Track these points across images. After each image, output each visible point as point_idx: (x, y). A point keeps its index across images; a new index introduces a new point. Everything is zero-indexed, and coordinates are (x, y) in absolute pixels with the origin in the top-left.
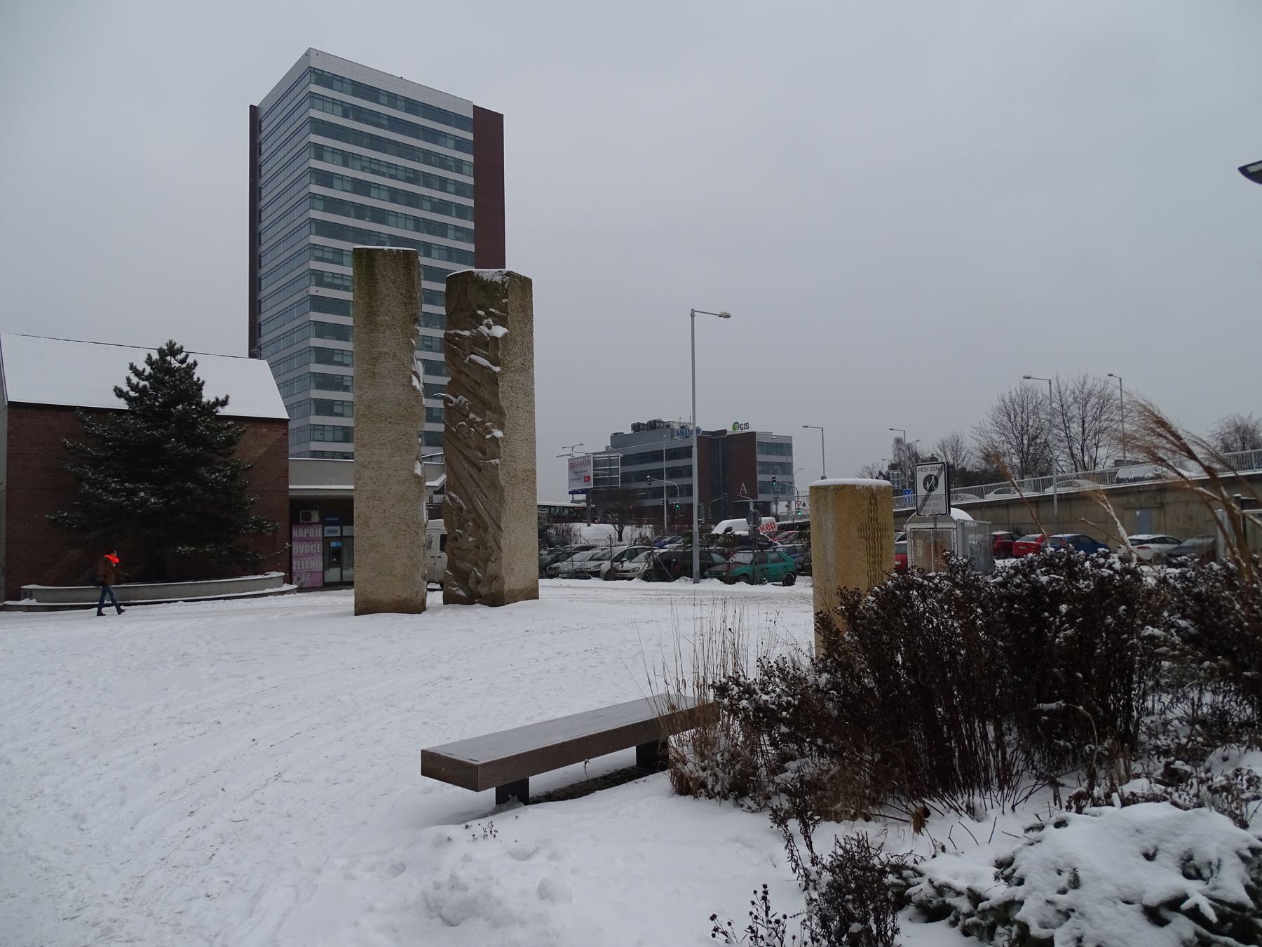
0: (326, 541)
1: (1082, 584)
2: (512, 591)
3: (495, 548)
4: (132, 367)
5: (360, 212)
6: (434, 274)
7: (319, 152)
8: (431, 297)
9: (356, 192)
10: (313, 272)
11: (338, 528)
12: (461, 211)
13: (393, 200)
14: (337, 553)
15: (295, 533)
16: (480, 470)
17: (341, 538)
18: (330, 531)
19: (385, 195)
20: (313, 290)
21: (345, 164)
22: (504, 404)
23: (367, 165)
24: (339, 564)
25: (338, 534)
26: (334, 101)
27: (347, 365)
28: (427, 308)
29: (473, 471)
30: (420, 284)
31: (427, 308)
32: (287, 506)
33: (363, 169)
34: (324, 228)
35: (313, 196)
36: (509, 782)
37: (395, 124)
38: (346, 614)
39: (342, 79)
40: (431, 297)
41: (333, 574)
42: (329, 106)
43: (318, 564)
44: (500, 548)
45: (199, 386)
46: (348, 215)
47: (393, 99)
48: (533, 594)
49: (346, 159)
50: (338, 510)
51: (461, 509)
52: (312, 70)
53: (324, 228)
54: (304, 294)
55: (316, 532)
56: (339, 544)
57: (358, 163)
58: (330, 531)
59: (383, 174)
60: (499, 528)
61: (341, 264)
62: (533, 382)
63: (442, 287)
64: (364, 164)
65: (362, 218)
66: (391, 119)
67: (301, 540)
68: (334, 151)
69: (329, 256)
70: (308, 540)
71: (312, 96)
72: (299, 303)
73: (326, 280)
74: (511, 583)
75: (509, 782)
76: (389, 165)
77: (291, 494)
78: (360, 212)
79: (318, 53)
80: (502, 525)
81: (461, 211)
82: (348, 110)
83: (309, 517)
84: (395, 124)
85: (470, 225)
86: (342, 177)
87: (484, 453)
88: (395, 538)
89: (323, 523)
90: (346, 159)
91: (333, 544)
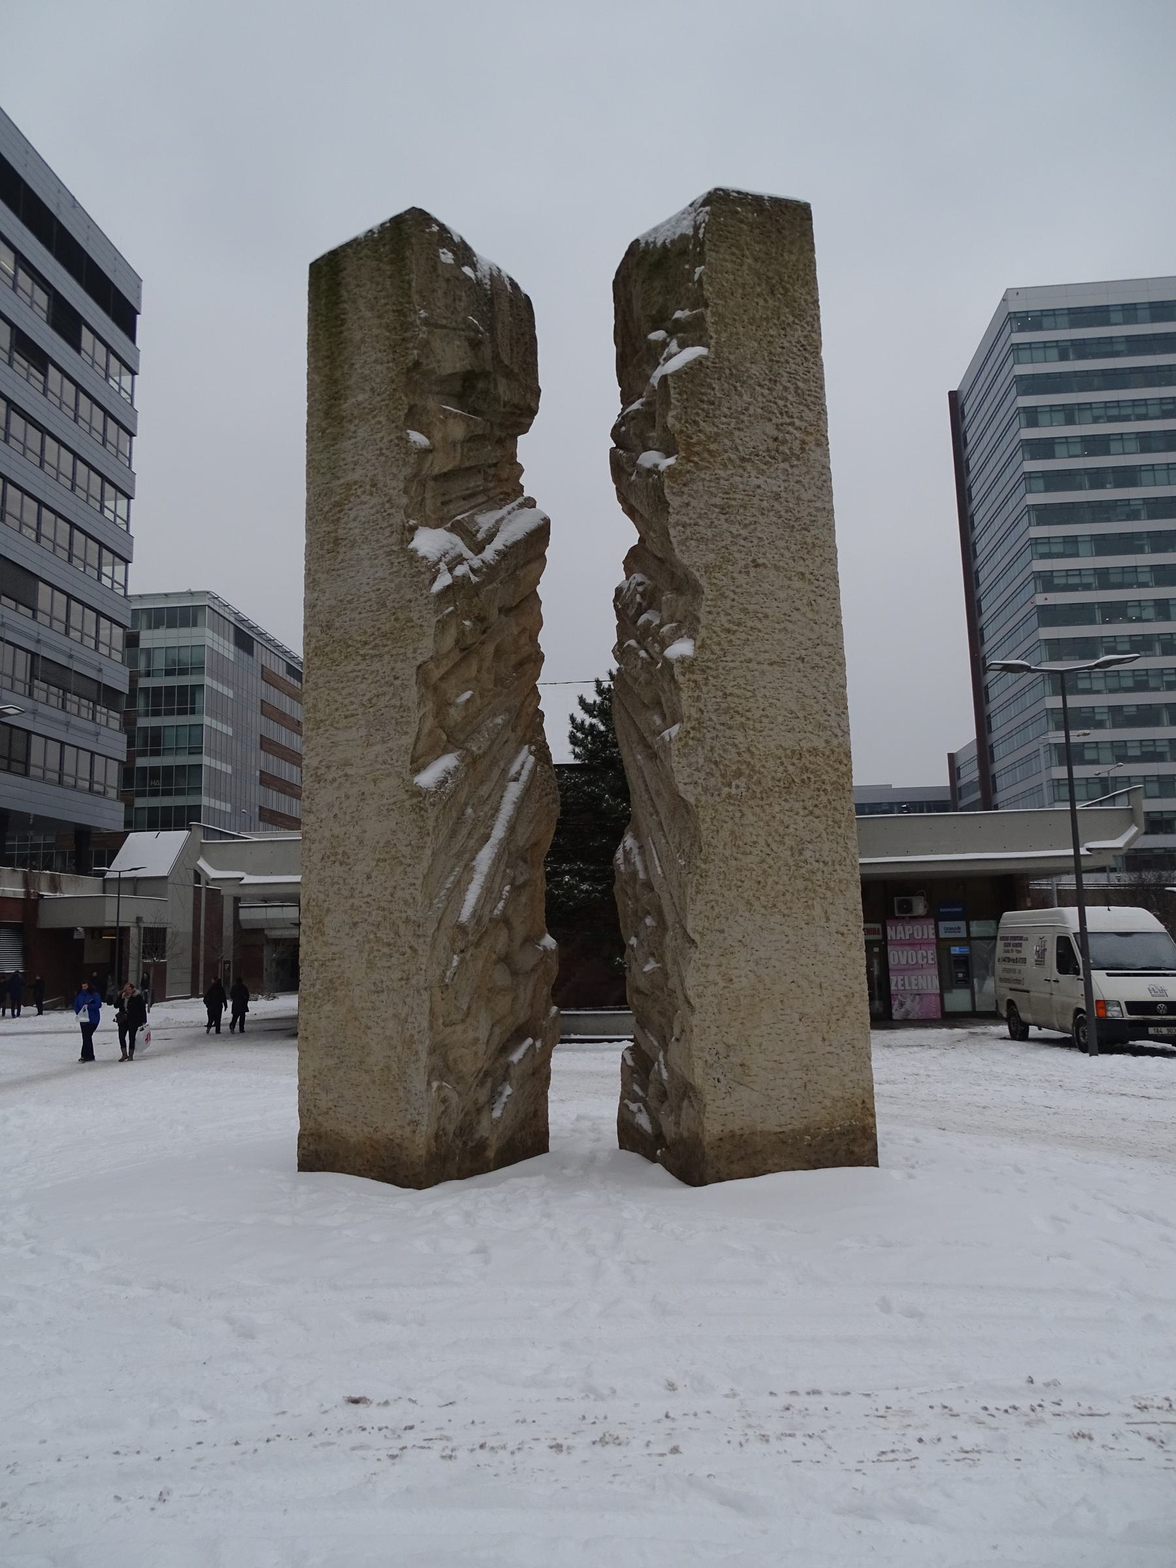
0: (942, 945)
1: (467, 270)
4: (582, 701)
5: (1097, 478)
7: (1032, 416)
9: (1092, 453)
10: (1038, 575)
11: (962, 924)
13: (1145, 449)
14: (963, 962)
15: (891, 933)
17: (968, 940)
18: (948, 930)
19: (1132, 445)
20: (1041, 599)
21: (1070, 421)
23: (1100, 412)
24: (967, 983)
25: (963, 934)
26: (1045, 345)
27: (1098, 692)
33: (1096, 420)
34: (1045, 514)
35: (1029, 476)
37: (1137, 345)
39: (1053, 313)
41: (958, 1000)
42: (1039, 354)
43: (930, 982)
46: (1080, 488)
47: (1130, 312)
49: (1070, 414)
52: (1012, 317)
53: (1045, 514)
54: (1029, 606)
55: (927, 931)
56: (965, 950)
57: (1088, 415)
58: (948, 930)
59: (1126, 418)
61: (1077, 555)
64: (1096, 413)
65: (1102, 486)
66: (1129, 339)
67: (902, 943)
68: (1052, 408)
69: (1057, 549)
70: (912, 943)
71: (1016, 348)
72: (1025, 620)
73: (1056, 581)
76: (1134, 403)
78: (1097, 478)
79: (1017, 292)
82: (1064, 350)
83: (907, 907)
84: (1137, 345)
86: (1066, 440)
89: (935, 915)
90: (1070, 414)
91: (955, 950)
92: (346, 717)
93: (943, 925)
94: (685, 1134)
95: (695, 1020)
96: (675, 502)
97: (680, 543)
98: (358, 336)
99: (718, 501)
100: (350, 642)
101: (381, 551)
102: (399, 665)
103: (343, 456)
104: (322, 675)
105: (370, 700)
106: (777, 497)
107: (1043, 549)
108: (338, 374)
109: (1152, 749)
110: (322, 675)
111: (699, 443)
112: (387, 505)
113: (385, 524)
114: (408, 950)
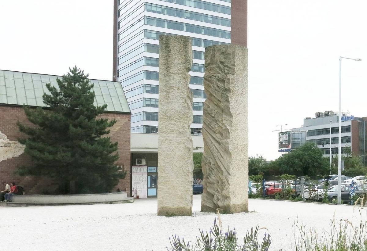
2: (234, 206)
3: (226, 182)
6: (198, 42)
8: (197, 55)
12: (224, 21)
16: (220, 144)
18: (150, 169)
22: (232, 111)
28: (195, 61)
29: (216, 145)
30: (191, 48)
31: (195, 61)
32: (129, 157)
36: (252, 229)
38: (152, 215)
40: (197, 55)
44: (229, 184)
45: (92, 96)
48: (245, 209)
50: (151, 159)
51: (210, 163)
60: (229, 173)
62: (247, 100)
63: (203, 49)
69: (154, 9)
74: (234, 201)
75: (252, 229)
77: (132, 150)
80: (230, 172)
81: (224, 21)
83: (140, 162)
85: (229, 29)
87: (222, 135)
88: (178, 177)
92: (171, 132)
93: (149, 168)
94: (225, 205)
95: (230, 187)
96: (230, 101)
97: (231, 109)
98: (174, 57)
99: (235, 102)
100: (172, 117)
101: (180, 102)
102: (184, 124)
103: (170, 80)
104: (164, 123)
105: (177, 129)
106: (242, 101)
107: (149, 8)
108: (169, 63)
109: (197, 106)
110: (164, 123)
111: (234, 91)
112: (182, 93)
113: (181, 97)
114: (186, 175)
